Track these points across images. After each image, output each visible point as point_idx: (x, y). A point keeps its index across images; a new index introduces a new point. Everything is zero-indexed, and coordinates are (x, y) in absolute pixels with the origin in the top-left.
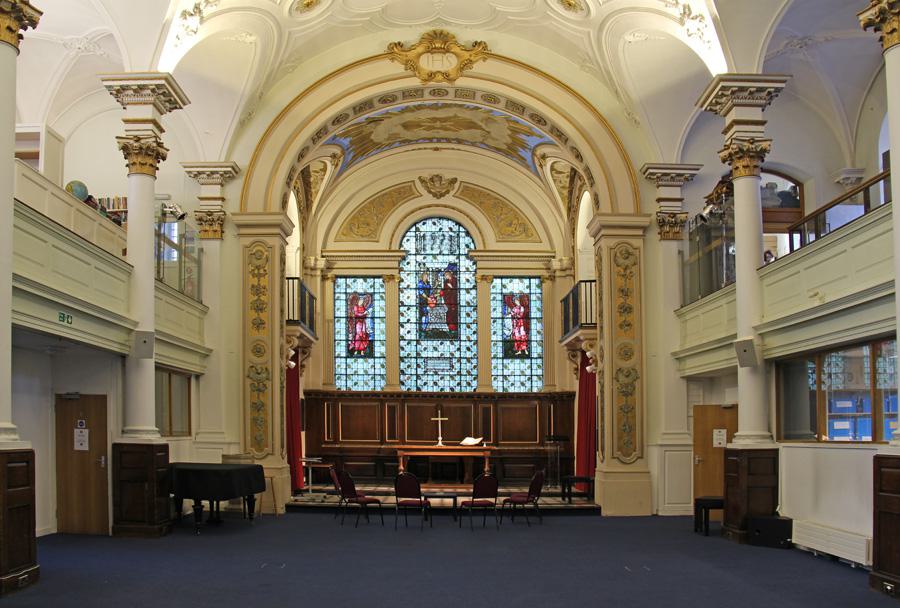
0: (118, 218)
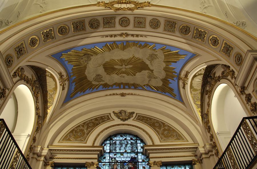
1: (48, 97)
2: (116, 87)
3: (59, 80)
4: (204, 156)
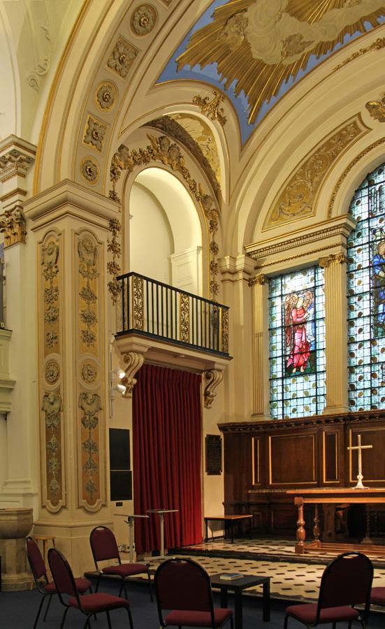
0: (94, 265)
1: (205, 153)
2: (351, 35)
3: (203, 112)
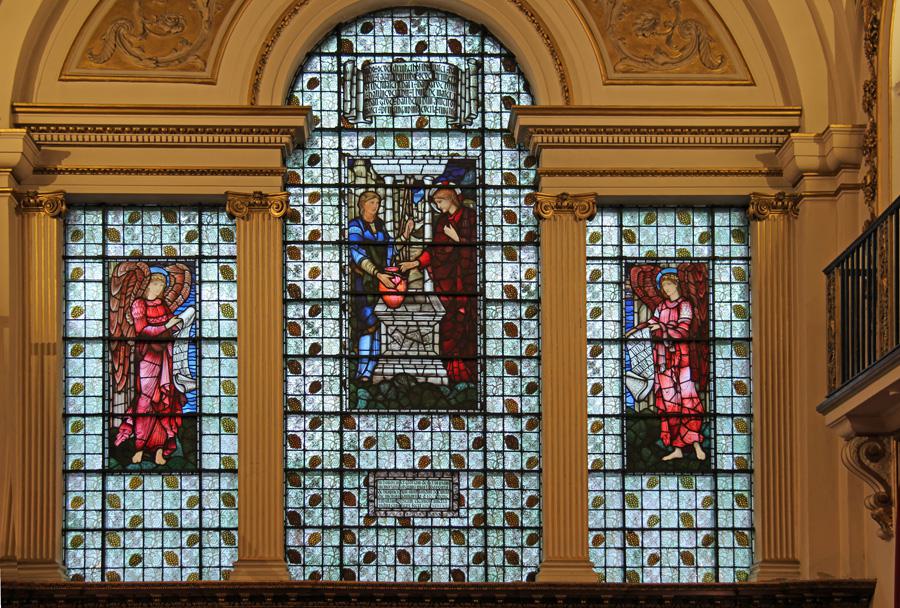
4: (809, 185)
